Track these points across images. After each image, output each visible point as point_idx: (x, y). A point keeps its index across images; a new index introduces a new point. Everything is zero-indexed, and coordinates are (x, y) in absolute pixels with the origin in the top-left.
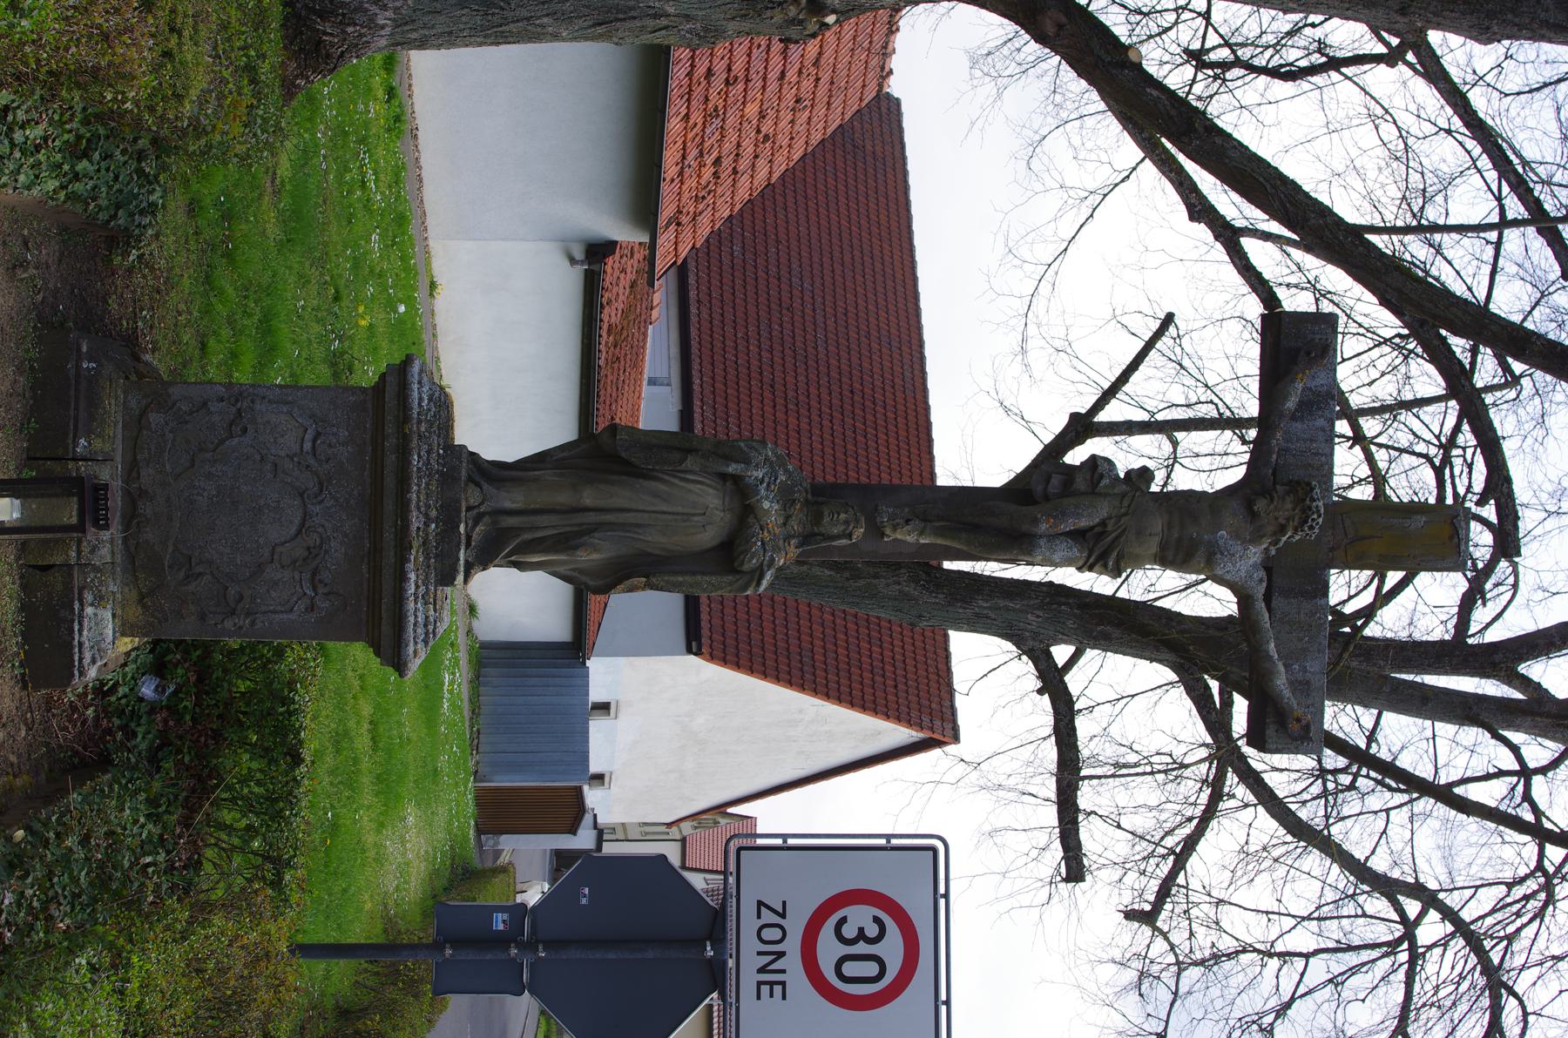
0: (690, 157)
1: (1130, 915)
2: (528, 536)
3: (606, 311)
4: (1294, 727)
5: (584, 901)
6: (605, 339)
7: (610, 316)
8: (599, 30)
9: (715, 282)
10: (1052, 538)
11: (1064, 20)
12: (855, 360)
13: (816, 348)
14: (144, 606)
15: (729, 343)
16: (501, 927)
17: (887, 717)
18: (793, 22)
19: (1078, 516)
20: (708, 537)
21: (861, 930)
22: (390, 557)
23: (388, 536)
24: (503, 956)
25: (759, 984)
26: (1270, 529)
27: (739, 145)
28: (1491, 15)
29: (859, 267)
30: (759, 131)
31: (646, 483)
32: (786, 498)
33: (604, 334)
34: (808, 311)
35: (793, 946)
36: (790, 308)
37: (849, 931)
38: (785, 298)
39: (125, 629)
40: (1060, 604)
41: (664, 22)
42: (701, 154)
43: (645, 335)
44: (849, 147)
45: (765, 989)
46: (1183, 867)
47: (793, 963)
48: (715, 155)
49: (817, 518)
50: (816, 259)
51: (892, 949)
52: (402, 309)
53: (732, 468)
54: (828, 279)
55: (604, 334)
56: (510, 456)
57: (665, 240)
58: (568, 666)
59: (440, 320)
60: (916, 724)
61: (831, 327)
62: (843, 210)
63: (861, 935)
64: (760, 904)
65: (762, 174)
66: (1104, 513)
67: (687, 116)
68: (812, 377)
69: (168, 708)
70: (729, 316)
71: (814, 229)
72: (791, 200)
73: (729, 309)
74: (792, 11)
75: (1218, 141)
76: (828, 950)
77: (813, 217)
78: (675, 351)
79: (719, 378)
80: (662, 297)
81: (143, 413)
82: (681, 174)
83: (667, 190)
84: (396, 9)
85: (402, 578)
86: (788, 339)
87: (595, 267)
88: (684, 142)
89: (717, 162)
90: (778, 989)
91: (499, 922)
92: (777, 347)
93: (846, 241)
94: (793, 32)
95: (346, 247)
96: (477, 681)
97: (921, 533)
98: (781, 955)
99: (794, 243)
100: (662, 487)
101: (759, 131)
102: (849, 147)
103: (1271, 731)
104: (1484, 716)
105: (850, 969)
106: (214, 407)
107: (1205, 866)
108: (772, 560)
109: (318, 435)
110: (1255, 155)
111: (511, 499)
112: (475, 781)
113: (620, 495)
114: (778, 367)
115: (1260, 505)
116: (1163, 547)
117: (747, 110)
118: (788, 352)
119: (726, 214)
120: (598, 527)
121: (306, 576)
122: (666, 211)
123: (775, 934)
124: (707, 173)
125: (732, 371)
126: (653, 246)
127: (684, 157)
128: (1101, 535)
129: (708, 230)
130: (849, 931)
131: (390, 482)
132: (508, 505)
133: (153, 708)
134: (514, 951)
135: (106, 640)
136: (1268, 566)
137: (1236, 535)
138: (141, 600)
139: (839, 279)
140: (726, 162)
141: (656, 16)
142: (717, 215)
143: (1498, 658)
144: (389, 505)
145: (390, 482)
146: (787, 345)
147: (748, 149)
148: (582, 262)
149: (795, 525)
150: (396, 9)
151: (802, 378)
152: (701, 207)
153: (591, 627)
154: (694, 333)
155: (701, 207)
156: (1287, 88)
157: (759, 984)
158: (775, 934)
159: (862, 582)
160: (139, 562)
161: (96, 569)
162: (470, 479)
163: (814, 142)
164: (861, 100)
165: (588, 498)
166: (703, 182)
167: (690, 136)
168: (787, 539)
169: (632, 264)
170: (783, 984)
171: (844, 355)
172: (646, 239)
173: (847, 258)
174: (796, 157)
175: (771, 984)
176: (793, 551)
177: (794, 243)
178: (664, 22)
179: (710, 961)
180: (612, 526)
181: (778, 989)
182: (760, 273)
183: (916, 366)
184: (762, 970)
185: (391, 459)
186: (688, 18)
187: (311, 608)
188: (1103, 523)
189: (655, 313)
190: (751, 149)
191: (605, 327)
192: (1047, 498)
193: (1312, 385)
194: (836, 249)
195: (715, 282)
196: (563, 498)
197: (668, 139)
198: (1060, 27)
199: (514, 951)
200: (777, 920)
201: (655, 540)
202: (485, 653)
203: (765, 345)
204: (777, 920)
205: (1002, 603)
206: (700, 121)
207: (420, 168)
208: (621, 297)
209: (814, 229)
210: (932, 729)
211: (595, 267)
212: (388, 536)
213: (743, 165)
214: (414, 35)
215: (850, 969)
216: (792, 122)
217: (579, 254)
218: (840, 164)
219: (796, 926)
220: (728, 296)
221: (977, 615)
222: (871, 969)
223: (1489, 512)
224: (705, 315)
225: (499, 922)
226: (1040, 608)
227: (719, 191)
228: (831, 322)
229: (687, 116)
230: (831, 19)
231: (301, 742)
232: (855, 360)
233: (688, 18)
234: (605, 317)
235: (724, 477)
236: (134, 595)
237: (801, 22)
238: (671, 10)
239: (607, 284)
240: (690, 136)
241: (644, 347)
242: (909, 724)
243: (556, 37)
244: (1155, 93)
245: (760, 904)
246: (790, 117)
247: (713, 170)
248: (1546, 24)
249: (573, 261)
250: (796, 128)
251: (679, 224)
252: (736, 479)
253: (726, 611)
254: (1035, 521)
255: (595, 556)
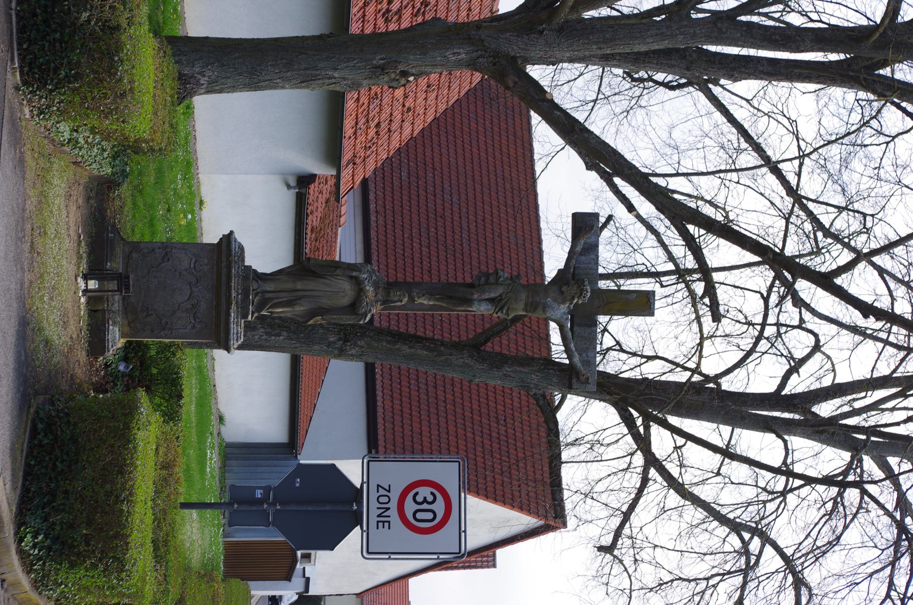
0: (360, 124)
1: (601, 549)
2: (276, 301)
3: (310, 217)
4: (582, 378)
5: (297, 485)
6: (309, 236)
7: (313, 221)
8: (303, 84)
9: (388, 198)
10: (480, 301)
11: (517, 80)
12: (490, 253)
13: (462, 245)
14: (130, 327)
15: (399, 241)
16: (259, 496)
17: (512, 507)
18: (394, 80)
19: (490, 292)
20: (346, 301)
21: (425, 498)
22: (224, 307)
23: (223, 299)
24: (260, 508)
25: (378, 522)
26: (569, 298)
27: (391, 115)
28: (733, 69)
29: (493, 185)
30: (404, 106)
31: (323, 280)
32: (376, 286)
33: (309, 232)
34: (456, 218)
35: (393, 505)
36: (443, 217)
37: (419, 499)
38: (439, 210)
39: (123, 335)
40: (549, 369)
41: (333, 81)
42: (368, 121)
43: (336, 234)
44: (487, 100)
45: (381, 524)
46: (629, 518)
47: (393, 513)
48: (376, 121)
49: (388, 294)
50: (462, 181)
51: (439, 507)
52: (190, 216)
53: (354, 274)
54: (471, 195)
55: (309, 232)
56: (269, 272)
57: (346, 174)
58: (286, 459)
59: (204, 225)
60: (534, 513)
61: (473, 230)
62: (482, 146)
63: (425, 500)
64: (378, 486)
65: (407, 131)
66: (501, 292)
67: (358, 99)
68: (459, 265)
69: (129, 375)
70: (398, 222)
71: (460, 160)
72: (443, 138)
73: (398, 217)
74: (393, 76)
75: (586, 135)
76: (410, 507)
77: (460, 151)
78: (360, 247)
79: (391, 266)
80: (349, 209)
81: (130, 253)
82: (355, 133)
83: (346, 144)
84: (209, 77)
85: (229, 315)
86: (441, 238)
87: (303, 191)
88: (357, 115)
89: (378, 125)
90: (386, 524)
91: (259, 494)
92: (433, 244)
93: (484, 168)
94: (394, 84)
95: (171, 184)
96: (224, 467)
97: (429, 300)
98: (388, 509)
99: (446, 170)
100: (327, 281)
101: (404, 106)
102: (487, 100)
103: (574, 381)
104: (776, 427)
105: (420, 516)
106: (157, 251)
107: (639, 517)
108: (370, 310)
109: (196, 261)
110: (604, 142)
111: (269, 287)
112: (225, 537)
113: (312, 285)
114: (434, 259)
115: (564, 288)
116: (526, 305)
117: (396, 94)
118: (440, 247)
119: (385, 157)
120: (300, 298)
121: (192, 315)
122: (346, 156)
123: (385, 499)
124: (372, 132)
125: (400, 261)
126: (338, 177)
127: (357, 123)
128: (501, 300)
129: (373, 167)
130: (419, 499)
131: (224, 279)
132: (268, 289)
133: (124, 375)
134: (265, 506)
135: (116, 339)
136: (571, 312)
137: (555, 300)
138: (129, 325)
139: (479, 195)
140: (383, 125)
141: (329, 78)
142: (379, 158)
143: (796, 401)
144: (224, 288)
145: (224, 279)
146: (441, 243)
147: (397, 116)
148: (295, 188)
149: (380, 297)
150: (209, 77)
151: (451, 266)
152: (368, 153)
153: (301, 432)
154: (373, 234)
155: (368, 153)
156: (672, 94)
157: (378, 522)
158: (385, 499)
159: (443, 358)
160: (128, 309)
161: (113, 312)
162: (253, 279)
163: (440, 110)
164: (471, 83)
165: (299, 285)
166: (369, 138)
167: (360, 111)
168: (377, 302)
169: (328, 188)
170: (389, 522)
171: (482, 249)
172: (334, 173)
173: (485, 180)
174: (429, 120)
175: (384, 522)
176: (379, 307)
177: (446, 170)
178: (333, 81)
179: (355, 511)
180: (309, 297)
181: (386, 524)
182: (421, 192)
183: (537, 257)
184: (379, 516)
185: (224, 270)
186: (344, 79)
187: (194, 327)
188: (501, 295)
189: (342, 220)
190: (399, 117)
191: (309, 228)
192: (479, 285)
193: (588, 241)
194: (477, 173)
195: (388, 198)
196: (290, 286)
197: (346, 113)
198: (516, 83)
199: (265, 506)
200: (386, 493)
201: (326, 302)
202: (229, 450)
203: (425, 242)
204: (386, 493)
205: (518, 369)
206: (366, 102)
207: (195, 131)
208: (320, 209)
209: (460, 160)
210: (546, 518)
211: (303, 191)
212: (223, 299)
213: (394, 127)
214: (217, 88)
215: (420, 516)
216: (426, 99)
217: (293, 183)
218: (480, 112)
219: (395, 496)
220: (397, 208)
221: (504, 375)
222: (429, 516)
223: (707, 300)
224: (381, 221)
225: (259, 494)
226: (539, 371)
227: (380, 142)
228: (473, 226)
229: (358, 99)
230: (411, 79)
231: (182, 390)
232: (490, 253)
233: (344, 79)
234: (310, 222)
235: (351, 277)
236: (126, 323)
237: (397, 80)
238: (337, 75)
239: (310, 201)
240: (360, 111)
241: (335, 242)
242: (529, 512)
243: (283, 87)
244: (558, 113)
245: (378, 486)
246: (424, 96)
247: (375, 130)
248: (762, 72)
249: (289, 187)
250: (428, 102)
251: (354, 164)
252: (356, 278)
253: (396, 428)
254: (472, 294)
255: (302, 308)
